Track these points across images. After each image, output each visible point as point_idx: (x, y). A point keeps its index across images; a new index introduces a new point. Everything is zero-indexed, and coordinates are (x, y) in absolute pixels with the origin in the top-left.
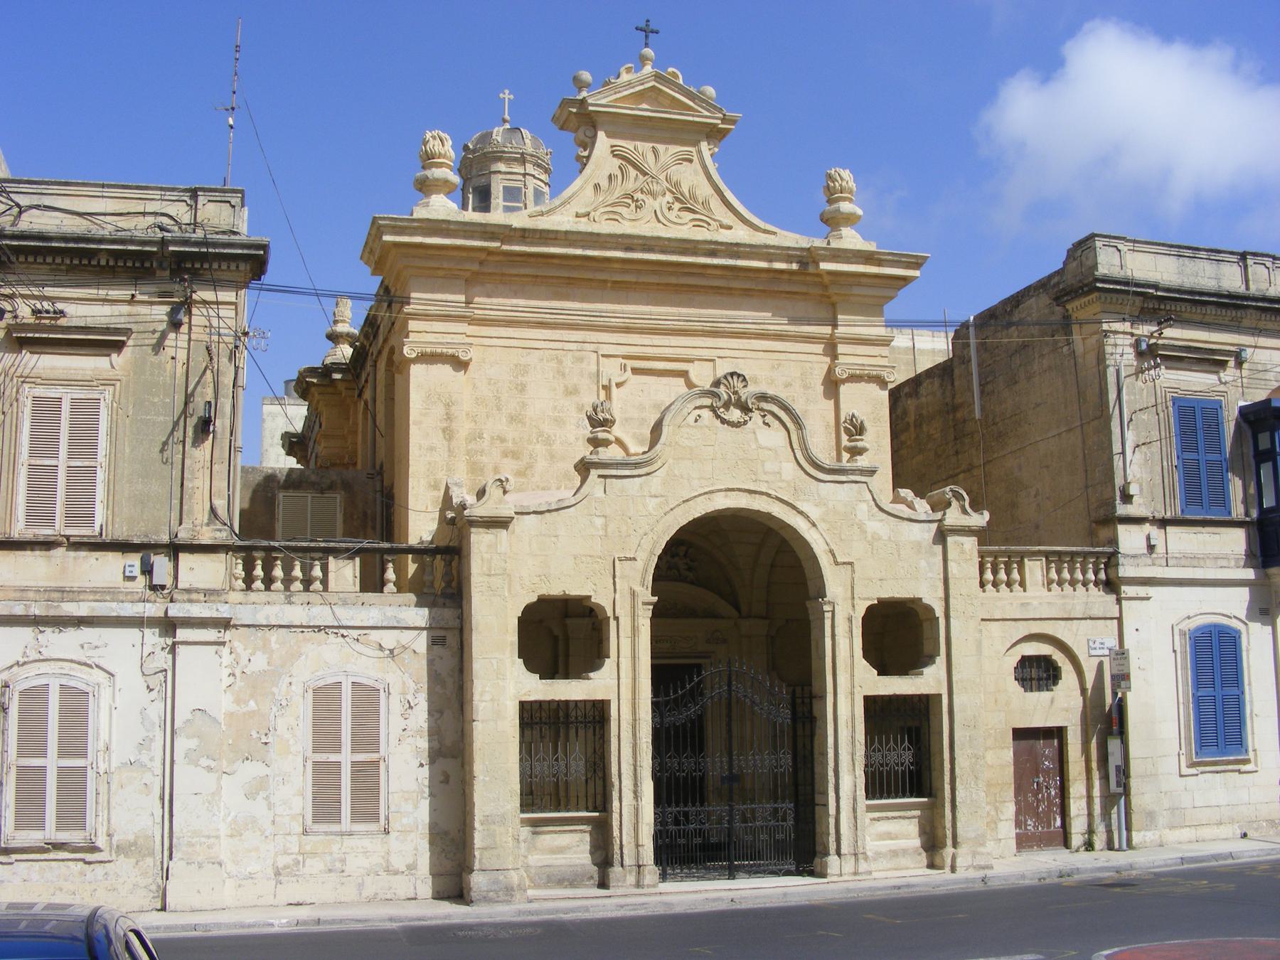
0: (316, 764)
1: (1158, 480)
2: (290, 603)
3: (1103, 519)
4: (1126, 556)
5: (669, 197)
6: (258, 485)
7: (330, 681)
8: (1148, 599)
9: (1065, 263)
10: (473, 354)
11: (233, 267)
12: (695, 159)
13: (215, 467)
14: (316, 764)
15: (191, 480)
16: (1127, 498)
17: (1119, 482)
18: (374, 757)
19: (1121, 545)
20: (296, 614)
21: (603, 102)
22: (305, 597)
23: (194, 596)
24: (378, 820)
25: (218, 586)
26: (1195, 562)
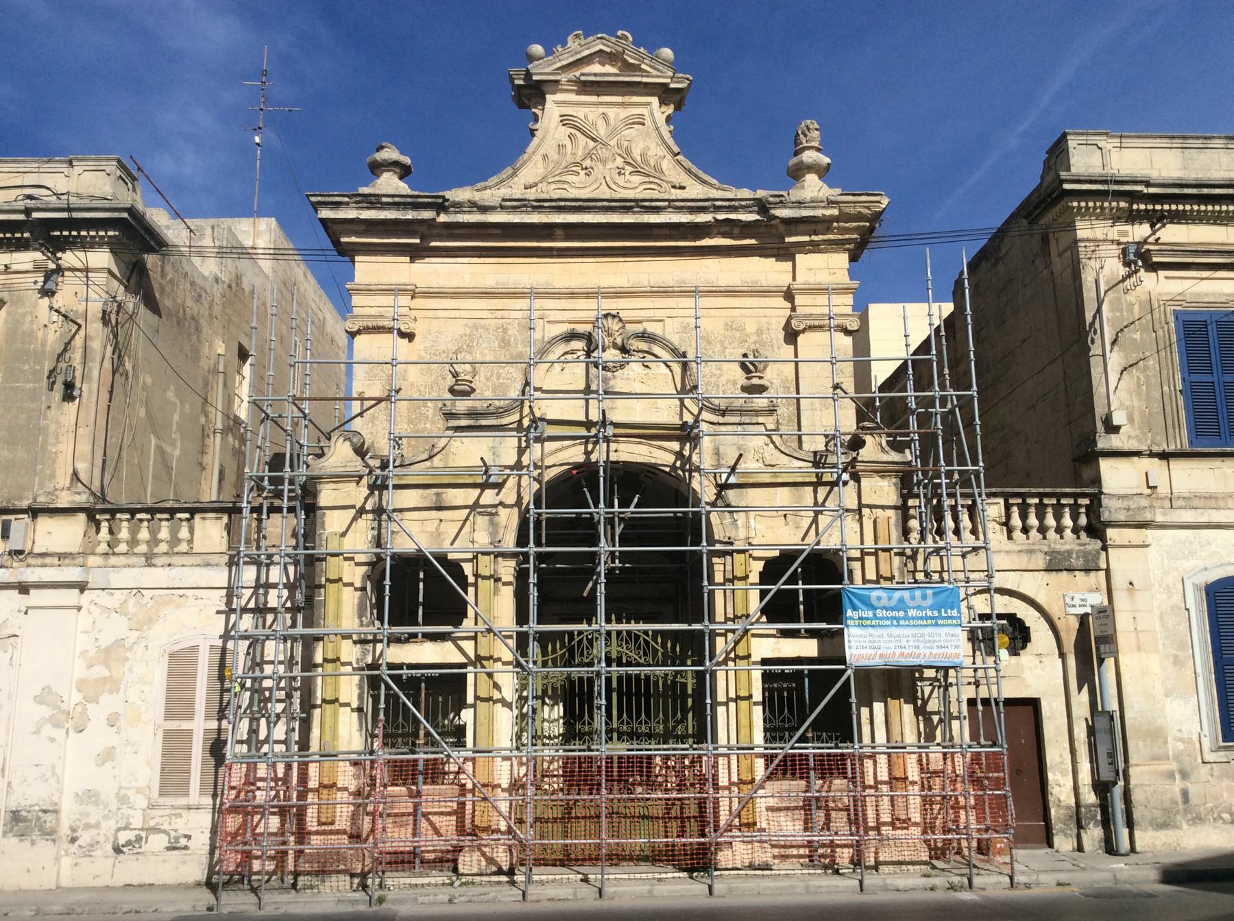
1: (1157, 407)
2: (150, 565)
3: (1085, 457)
4: (1112, 496)
5: (619, 161)
7: (187, 644)
8: (1147, 546)
9: (1042, 178)
10: (418, 329)
12: (648, 122)
13: (80, 431)
15: (54, 445)
16: (1113, 429)
17: (1100, 411)
19: (1104, 484)
20: (157, 576)
21: (548, 70)
23: (48, 560)
25: (74, 550)
26: (1213, 503)
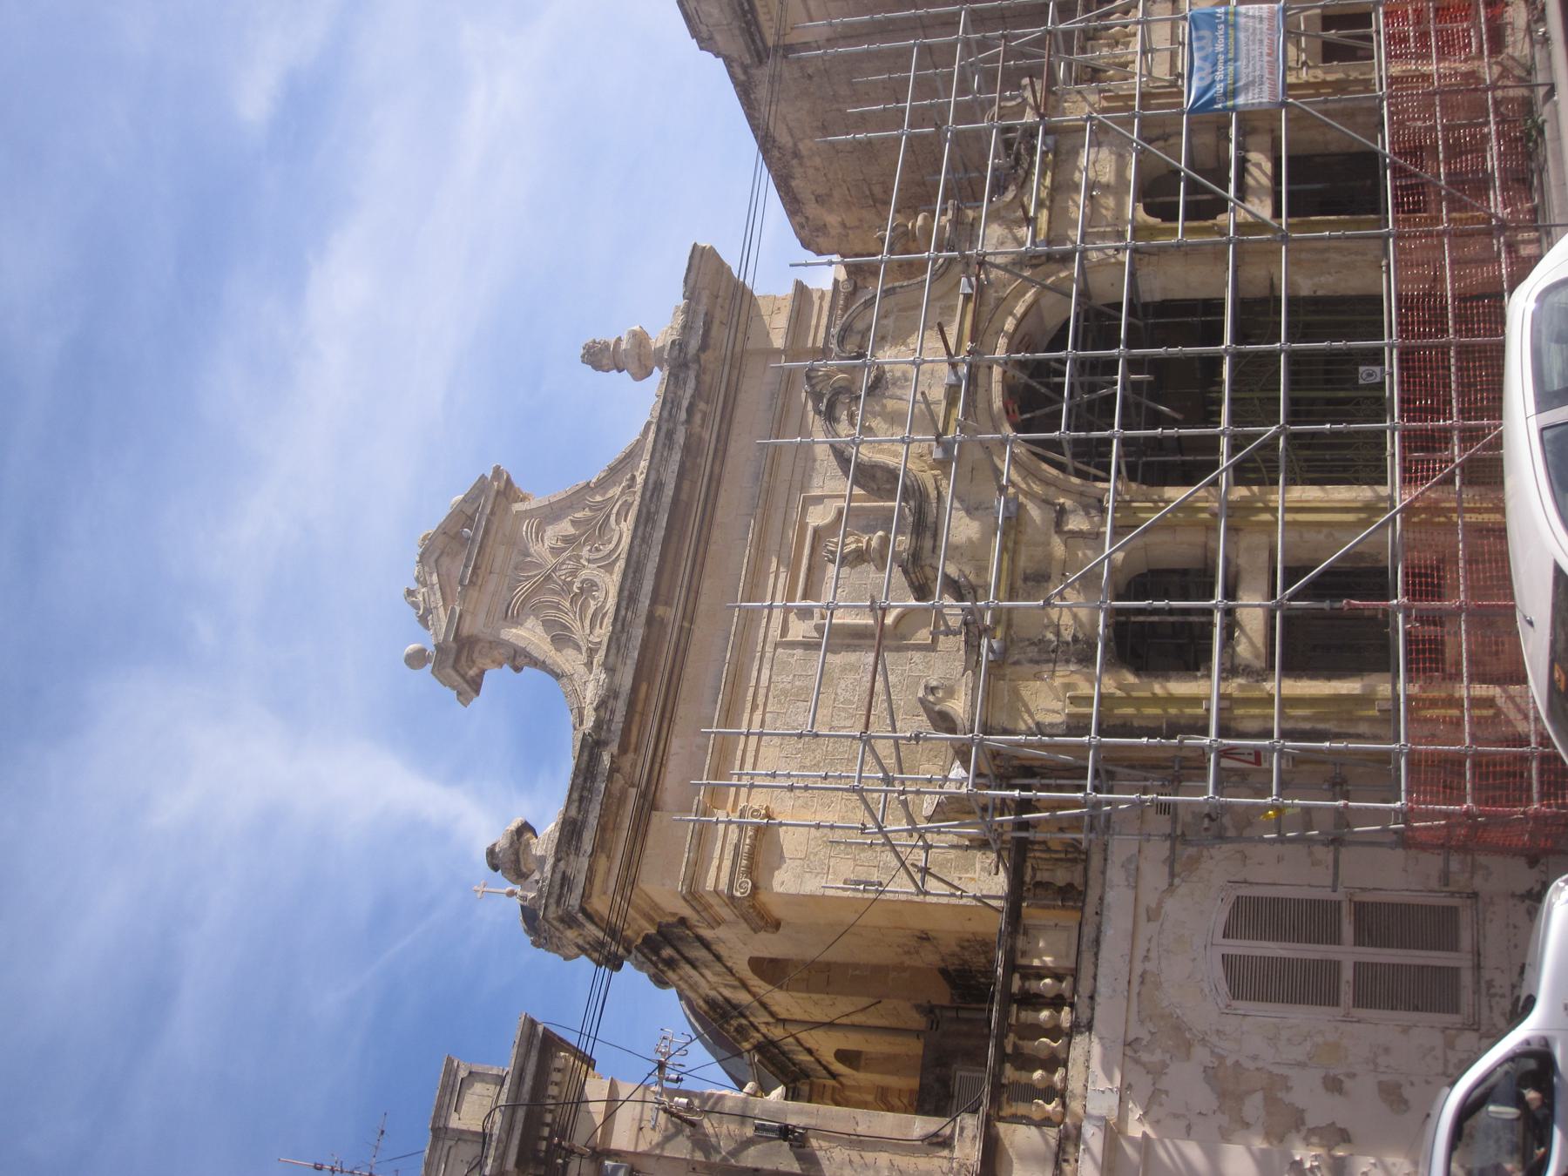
0: (1359, 1002)
6: (778, 868)
9: (717, 55)
11: (556, 1077)
14: (1359, 1002)
18: (1346, 910)
22: (1081, 1002)
24: (1454, 911)
